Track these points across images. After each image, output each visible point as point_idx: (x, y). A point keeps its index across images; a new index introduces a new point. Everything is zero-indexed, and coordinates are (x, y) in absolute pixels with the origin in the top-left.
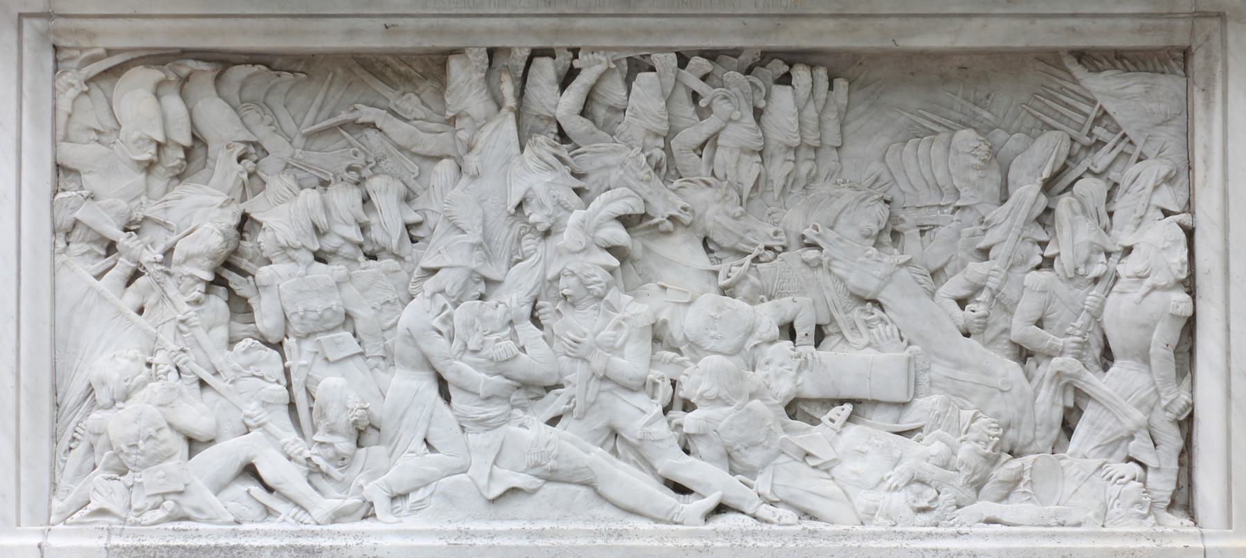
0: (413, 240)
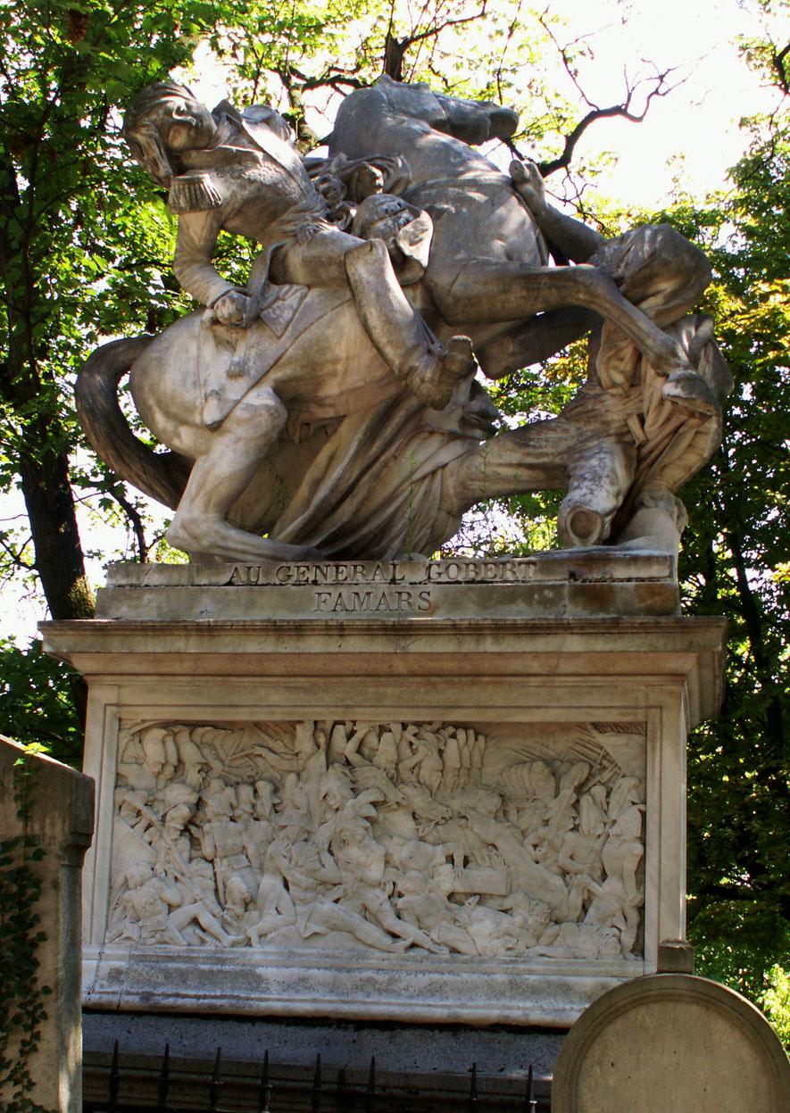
0: (277, 812)
